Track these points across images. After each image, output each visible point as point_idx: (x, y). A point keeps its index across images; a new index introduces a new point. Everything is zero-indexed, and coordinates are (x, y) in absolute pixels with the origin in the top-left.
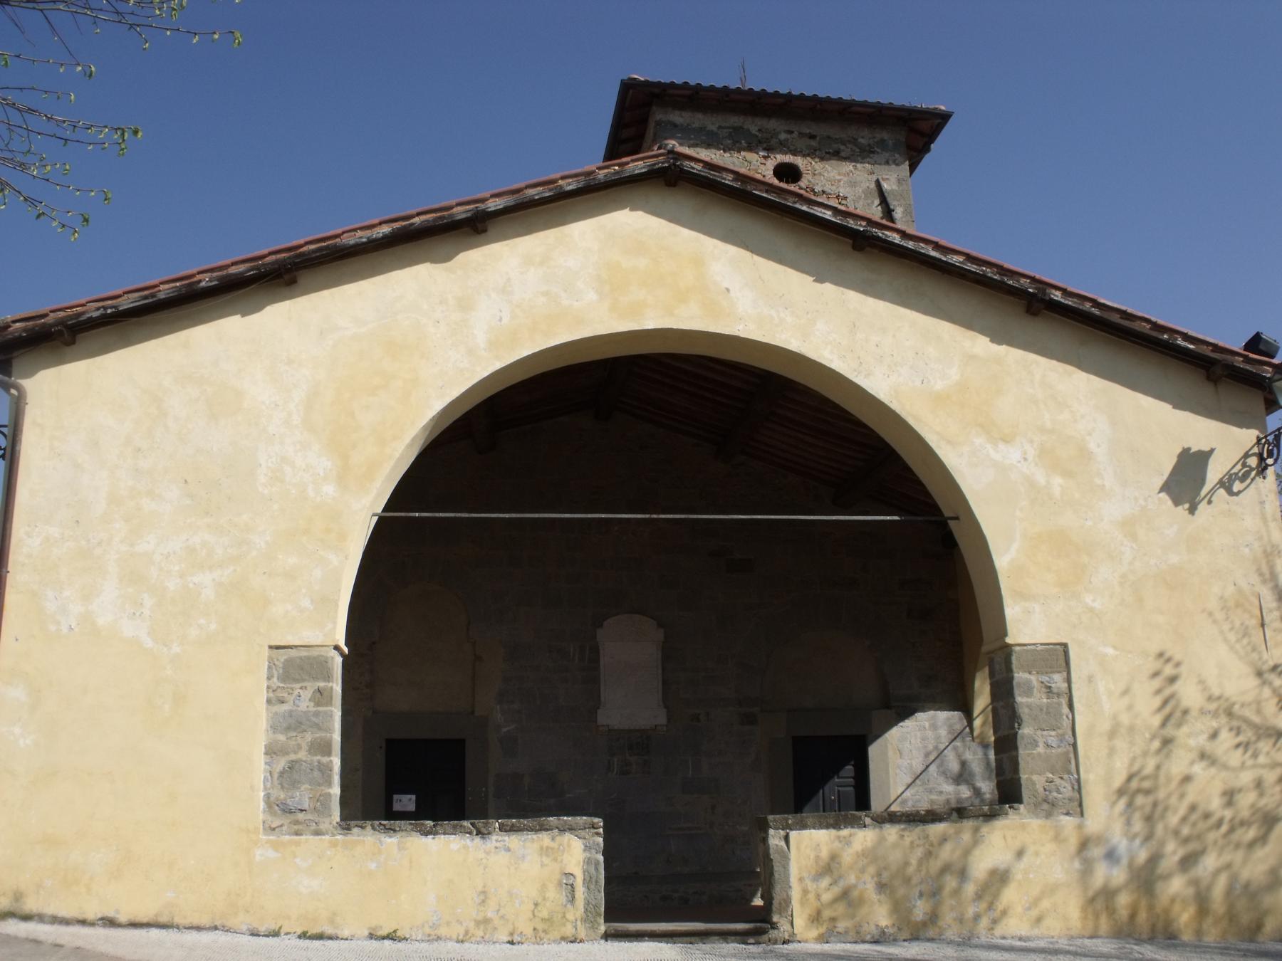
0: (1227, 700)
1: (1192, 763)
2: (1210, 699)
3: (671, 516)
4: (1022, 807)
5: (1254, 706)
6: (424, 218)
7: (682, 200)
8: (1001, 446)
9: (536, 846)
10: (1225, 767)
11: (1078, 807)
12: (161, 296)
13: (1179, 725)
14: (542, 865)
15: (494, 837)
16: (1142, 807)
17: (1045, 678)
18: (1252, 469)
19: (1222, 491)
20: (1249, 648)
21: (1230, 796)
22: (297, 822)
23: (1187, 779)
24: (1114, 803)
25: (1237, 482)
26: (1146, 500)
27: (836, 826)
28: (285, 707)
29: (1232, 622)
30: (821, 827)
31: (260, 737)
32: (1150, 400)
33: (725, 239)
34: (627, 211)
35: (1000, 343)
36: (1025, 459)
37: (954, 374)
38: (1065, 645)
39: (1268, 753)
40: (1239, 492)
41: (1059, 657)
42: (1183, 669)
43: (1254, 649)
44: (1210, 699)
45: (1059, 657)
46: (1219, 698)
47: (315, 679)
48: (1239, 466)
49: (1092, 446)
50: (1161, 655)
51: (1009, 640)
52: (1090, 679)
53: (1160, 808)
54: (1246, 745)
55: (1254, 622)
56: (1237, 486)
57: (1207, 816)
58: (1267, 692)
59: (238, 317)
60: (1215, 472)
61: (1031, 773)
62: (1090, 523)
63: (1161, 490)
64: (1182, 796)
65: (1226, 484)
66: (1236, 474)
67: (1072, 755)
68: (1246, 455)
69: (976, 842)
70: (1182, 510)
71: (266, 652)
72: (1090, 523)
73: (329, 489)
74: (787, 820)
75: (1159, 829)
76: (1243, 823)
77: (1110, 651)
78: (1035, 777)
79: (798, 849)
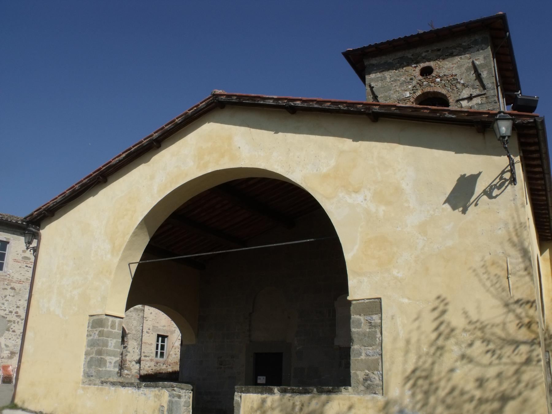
0: (482, 323)
1: (456, 361)
2: (470, 323)
3: (176, 258)
4: (349, 388)
5: (501, 326)
6: (135, 148)
7: (226, 113)
8: (354, 195)
9: (152, 394)
10: (478, 364)
11: (383, 389)
12: (67, 195)
13: (447, 338)
14: (155, 402)
15: (142, 389)
16: (422, 386)
17: (368, 318)
18: (507, 180)
19: (485, 197)
20: (500, 290)
21: (481, 382)
22: (90, 380)
23: (452, 370)
24: (405, 384)
25: (496, 190)
26: (434, 211)
27: (262, 393)
28: (91, 338)
29: (489, 274)
30: (255, 393)
31: (83, 348)
32: (441, 152)
33: (240, 125)
34: (207, 124)
35: (357, 141)
36: (365, 200)
37: (333, 163)
38: (380, 299)
39: (509, 357)
40: (497, 196)
41: (375, 306)
42: (450, 308)
43: (503, 290)
44: (470, 323)
45: (375, 306)
46: (477, 322)
47: (100, 327)
48: (498, 180)
49: (404, 186)
50: (438, 297)
51: (349, 298)
52: (393, 317)
53: (434, 387)
54: (494, 352)
55: (504, 273)
56: (495, 192)
57: (462, 393)
58: (511, 316)
59: (92, 197)
60: (481, 186)
61: (357, 370)
62: (399, 229)
63: (445, 203)
64: (449, 380)
65: (488, 193)
66: (495, 185)
67: (380, 361)
68: (503, 172)
69: (327, 402)
70: (458, 213)
71: (88, 317)
72: (399, 229)
73: (109, 256)
74: (242, 388)
75: (432, 400)
76: (487, 401)
77: (406, 301)
78: (358, 373)
79: (244, 402)
